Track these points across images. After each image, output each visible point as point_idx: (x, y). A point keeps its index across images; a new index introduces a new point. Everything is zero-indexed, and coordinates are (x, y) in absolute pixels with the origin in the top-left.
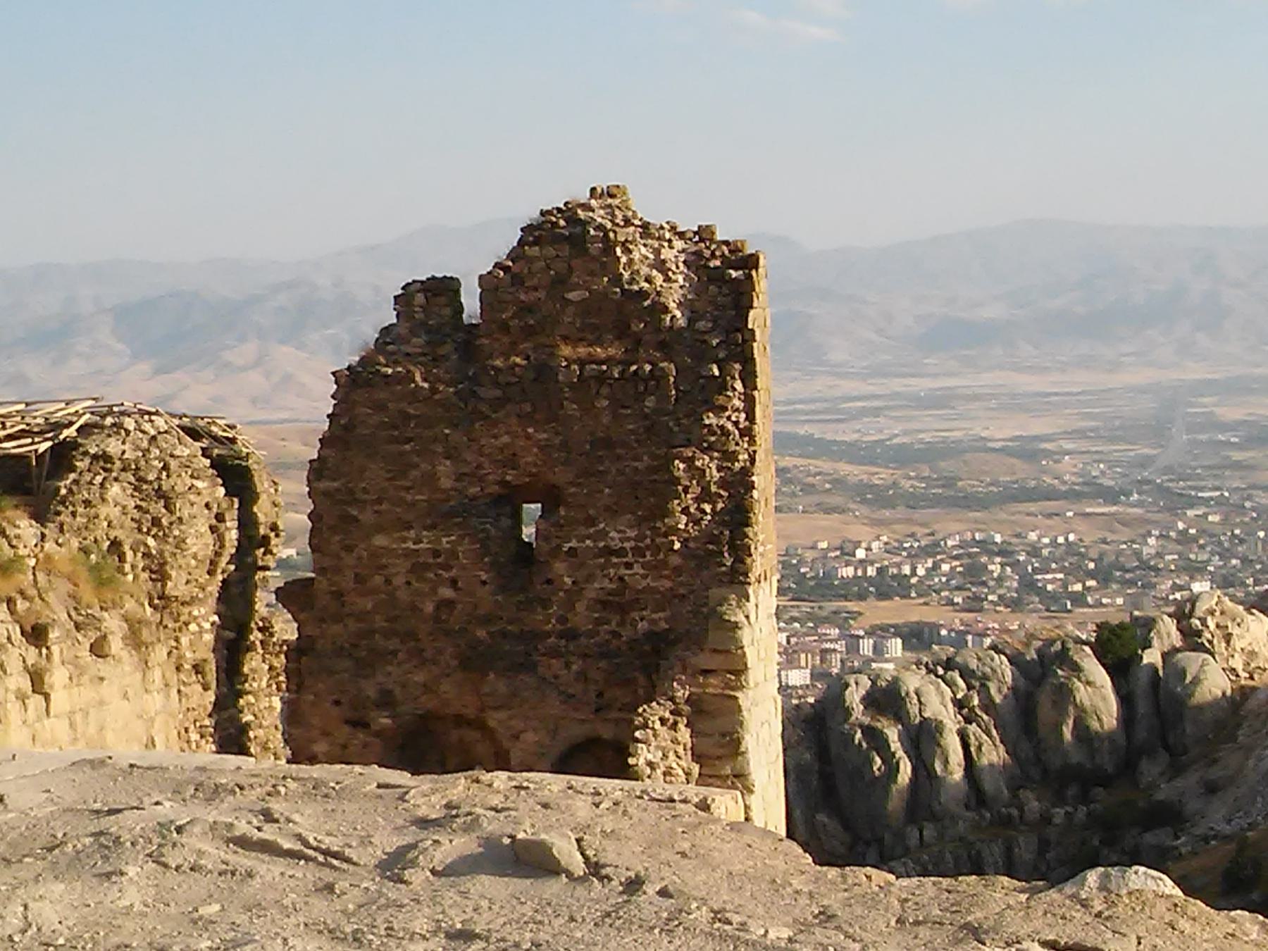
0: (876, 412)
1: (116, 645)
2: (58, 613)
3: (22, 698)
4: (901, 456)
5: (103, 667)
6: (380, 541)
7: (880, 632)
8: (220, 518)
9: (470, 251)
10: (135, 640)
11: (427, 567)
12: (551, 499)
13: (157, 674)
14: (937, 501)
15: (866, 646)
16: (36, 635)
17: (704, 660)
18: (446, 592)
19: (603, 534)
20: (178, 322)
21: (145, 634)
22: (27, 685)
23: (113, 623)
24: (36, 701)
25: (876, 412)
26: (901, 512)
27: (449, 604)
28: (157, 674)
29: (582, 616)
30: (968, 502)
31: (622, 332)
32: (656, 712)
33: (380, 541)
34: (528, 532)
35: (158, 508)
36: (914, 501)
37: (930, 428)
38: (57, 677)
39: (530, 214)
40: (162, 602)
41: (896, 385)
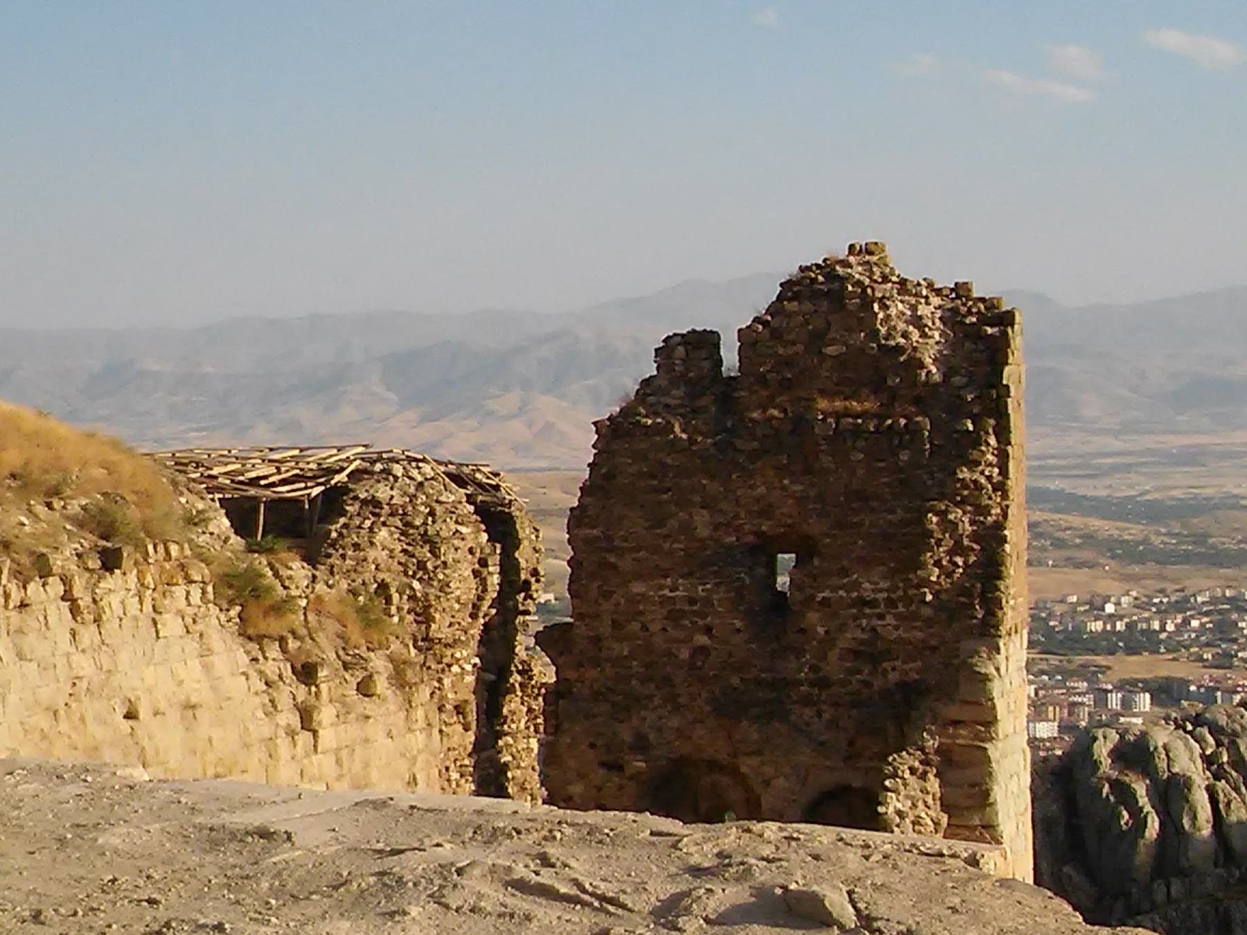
0: (1128, 468)
1: (381, 685)
2: (327, 651)
3: (292, 734)
4: (1153, 512)
5: (368, 706)
6: (638, 588)
7: (1129, 687)
8: (483, 563)
9: (730, 311)
10: (400, 680)
11: (682, 614)
12: (806, 551)
13: (420, 714)
14: (1186, 558)
15: (1115, 700)
16: (306, 673)
17: (954, 712)
18: (702, 639)
19: (856, 585)
20: (441, 372)
21: (410, 675)
22: (295, 721)
23: (378, 662)
24: (304, 738)
25: (1128, 468)
26: (1152, 568)
27: (703, 650)
28: (420, 714)
29: (834, 666)
30: (1218, 559)
31: (878, 387)
32: (906, 761)
33: (638, 588)
34: (783, 581)
35: (424, 552)
36: (1165, 558)
37: (1179, 485)
38: (326, 715)
39: (789, 269)
40: (426, 643)
41: (1149, 442)
